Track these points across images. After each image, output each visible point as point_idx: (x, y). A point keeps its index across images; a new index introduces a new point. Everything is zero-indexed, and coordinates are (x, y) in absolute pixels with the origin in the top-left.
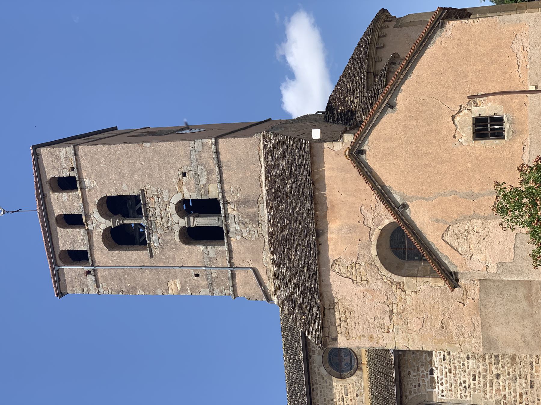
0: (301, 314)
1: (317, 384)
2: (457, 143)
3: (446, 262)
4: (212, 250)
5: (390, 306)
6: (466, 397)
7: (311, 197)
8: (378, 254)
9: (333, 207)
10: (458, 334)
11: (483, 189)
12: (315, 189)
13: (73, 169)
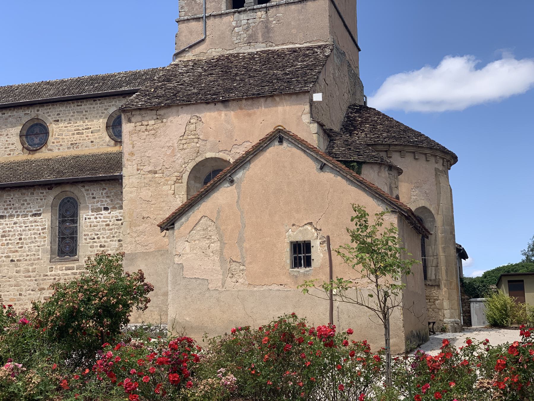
0: (156, 88)
1: (100, 104)
2: (288, 227)
5: (160, 171)
6: (86, 239)
7: (259, 94)
8: (207, 159)
9: (249, 115)
10: (138, 232)
11: (246, 251)
12: (266, 97)
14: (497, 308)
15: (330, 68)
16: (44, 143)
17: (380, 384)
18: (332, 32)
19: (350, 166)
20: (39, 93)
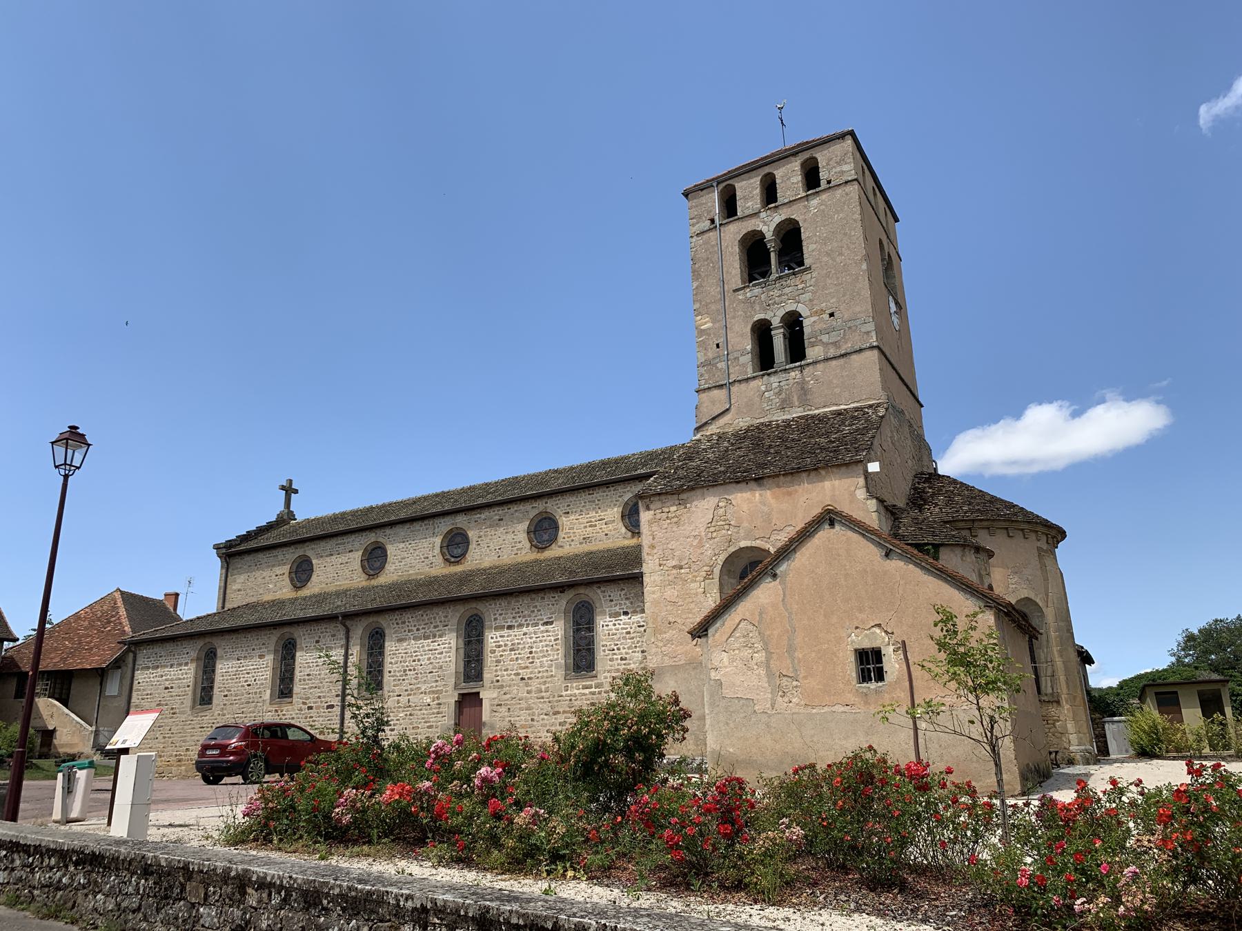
3: (718, 625)
4: (747, 359)
9: (790, 494)
13: (829, 182)
14: (1144, 732)
15: (886, 430)
16: (553, 539)
17: (995, 840)
18: (885, 388)
19: (925, 552)
20: (546, 483)
